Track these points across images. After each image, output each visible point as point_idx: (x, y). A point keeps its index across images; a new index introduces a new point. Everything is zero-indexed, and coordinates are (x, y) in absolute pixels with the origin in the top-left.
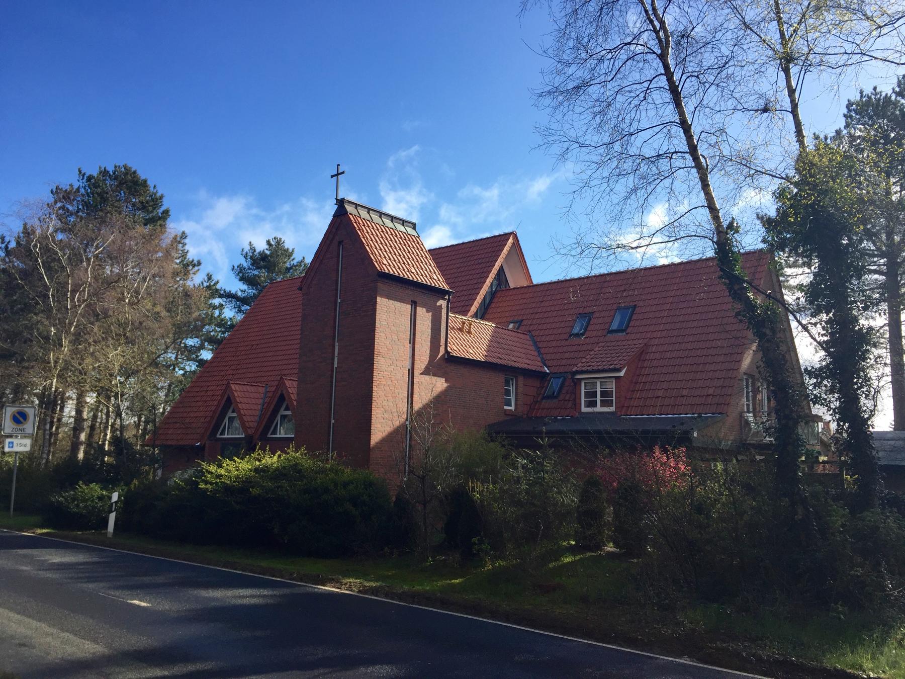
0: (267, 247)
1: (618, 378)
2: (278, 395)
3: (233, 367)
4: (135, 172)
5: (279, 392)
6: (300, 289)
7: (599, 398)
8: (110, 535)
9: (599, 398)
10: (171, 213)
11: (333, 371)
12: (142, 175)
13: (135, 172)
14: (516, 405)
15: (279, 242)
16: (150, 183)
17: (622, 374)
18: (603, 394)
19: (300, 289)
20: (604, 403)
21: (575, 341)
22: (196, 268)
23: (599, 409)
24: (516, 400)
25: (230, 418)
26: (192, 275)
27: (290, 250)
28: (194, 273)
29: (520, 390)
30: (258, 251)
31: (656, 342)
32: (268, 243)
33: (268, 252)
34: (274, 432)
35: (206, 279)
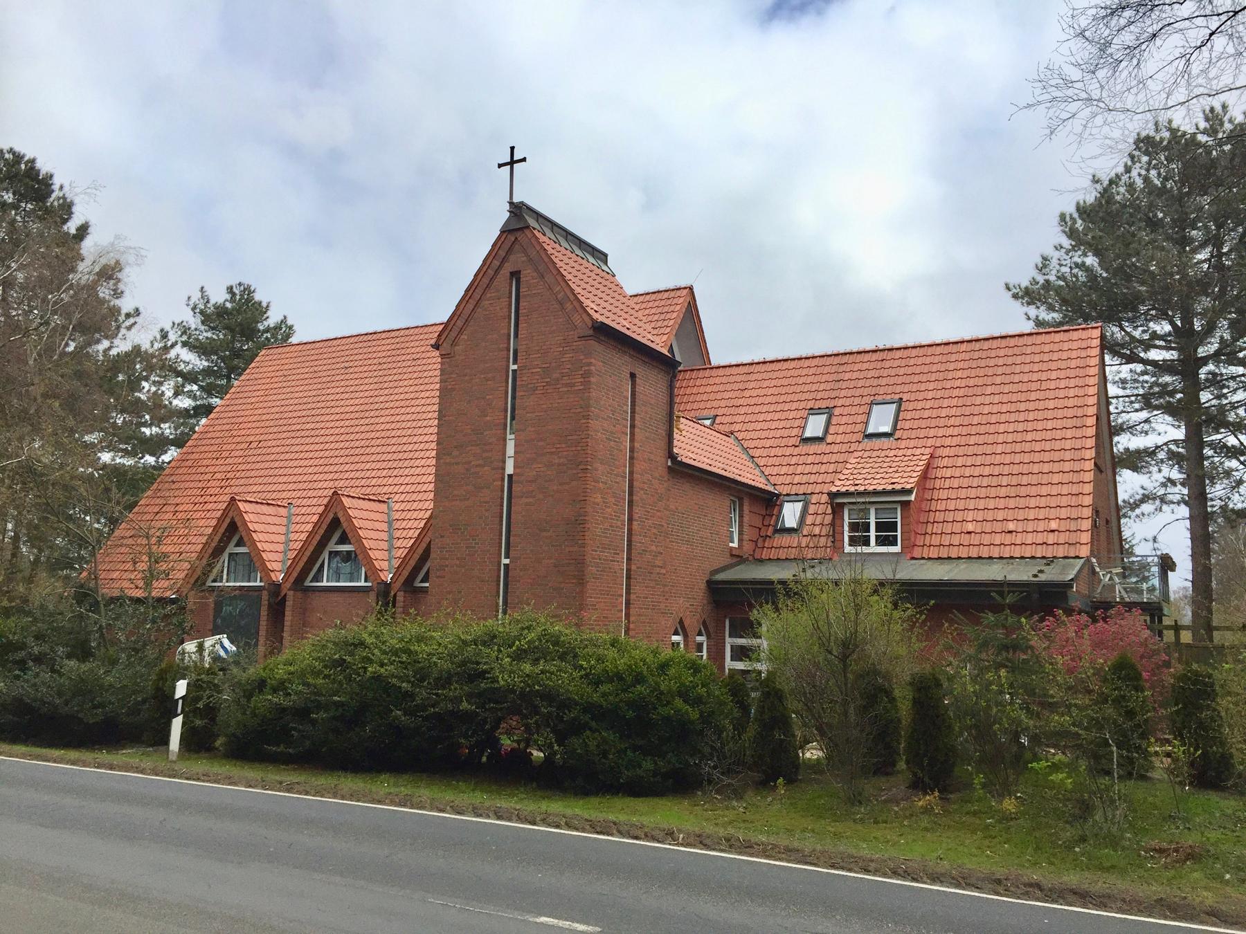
0: (228, 297)
1: (905, 505)
2: (328, 520)
3: (218, 476)
4: (33, 161)
5: (331, 516)
6: (436, 346)
7: (873, 533)
8: (173, 757)
9: (873, 533)
10: (90, 230)
11: (503, 480)
12: (43, 166)
13: (33, 161)
14: (740, 540)
15: (248, 291)
16: (57, 182)
17: (913, 498)
18: (880, 527)
19: (436, 346)
20: (881, 541)
21: (812, 448)
22: (132, 320)
23: (873, 548)
24: (741, 533)
25: (230, 555)
26: (123, 331)
27: (264, 304)
28: (129, 328)
29: (746, 519)
30: (212, 301)
31: (946, 452)
32: (230, 290)
33: (229, 305)
34: (318, 577)
35: (158, 337)
